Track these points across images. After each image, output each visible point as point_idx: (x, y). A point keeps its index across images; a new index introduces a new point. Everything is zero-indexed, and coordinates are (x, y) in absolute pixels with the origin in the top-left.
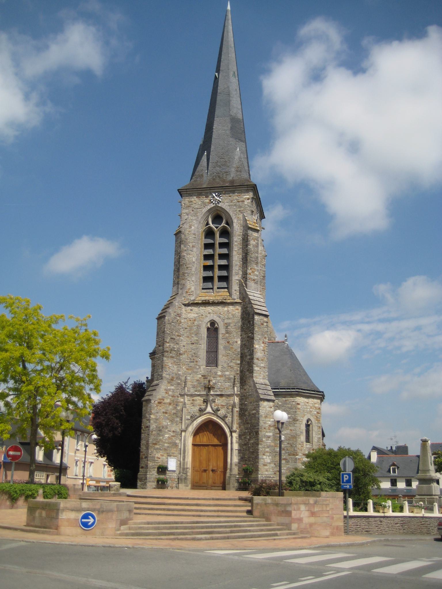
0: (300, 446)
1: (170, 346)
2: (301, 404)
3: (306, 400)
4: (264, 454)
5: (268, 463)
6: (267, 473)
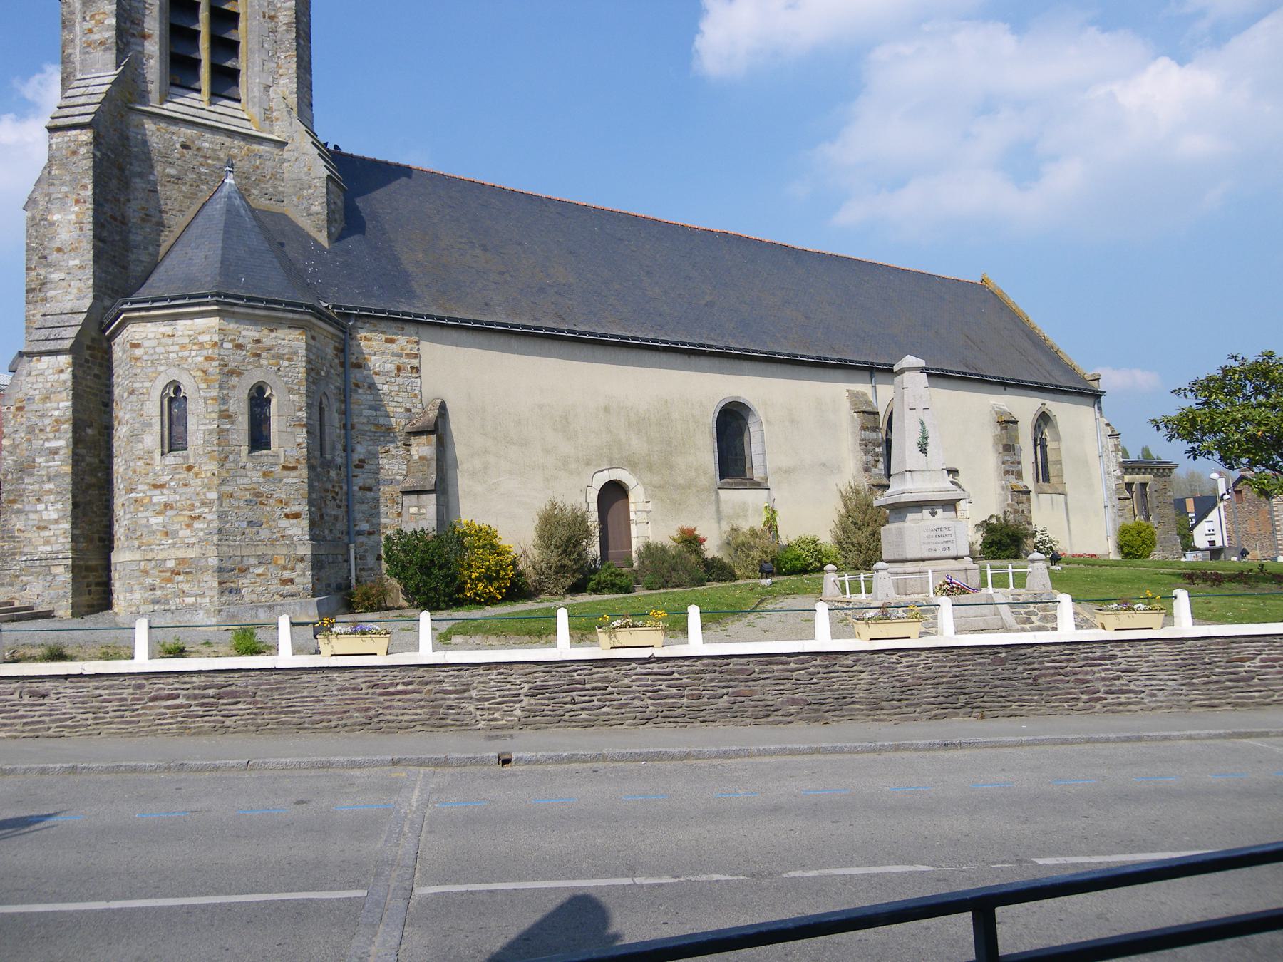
0: (141, 463)
1: (38, 275)
2: (146, 343)
3: (164, 328)
4: (39, 500)
5: (49, 521)
6: (48, 548)
